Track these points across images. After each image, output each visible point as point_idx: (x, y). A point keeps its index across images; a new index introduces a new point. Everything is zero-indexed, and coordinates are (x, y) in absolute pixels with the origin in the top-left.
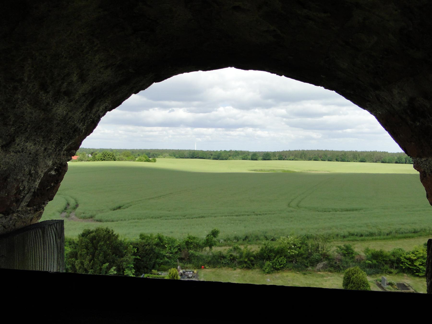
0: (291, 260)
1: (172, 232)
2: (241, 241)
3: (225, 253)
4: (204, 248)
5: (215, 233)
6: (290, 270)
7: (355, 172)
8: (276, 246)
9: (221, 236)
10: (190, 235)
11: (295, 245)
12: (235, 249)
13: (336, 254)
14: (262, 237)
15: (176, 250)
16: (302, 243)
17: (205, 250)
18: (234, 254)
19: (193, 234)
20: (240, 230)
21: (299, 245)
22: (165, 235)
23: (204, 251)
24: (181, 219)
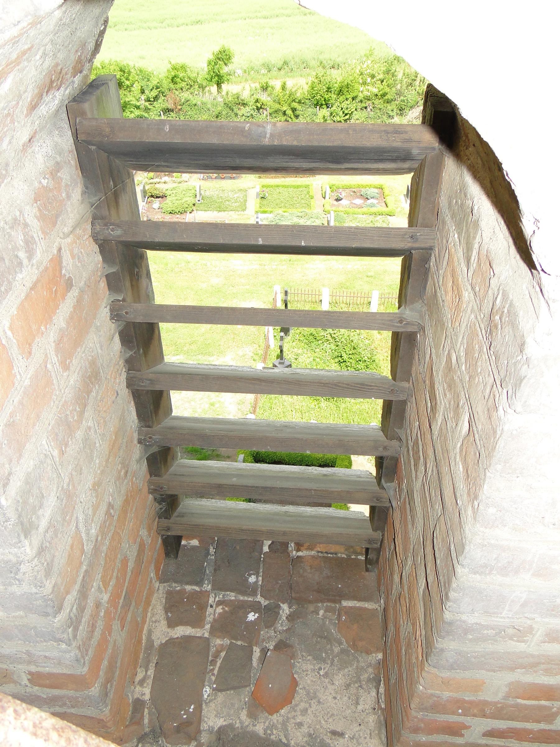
0: (364, 105)
1: (142, 58)
2: (274, 72)
3: (245, 96)
4: (207, 89)
5: (223, 57)
6: (203, 525)
7: (182, 304)
8: (337, 77)
9: (237, 65)
10: (173, 62)
11: (373, 76)
12: (265, 88)
13: (146, 126)
14: (313, 63)
15: (154, 93)
16: (388, 72)
17: (209, 91)
18: (264, 98)
19: (179, 61)
20: (274, 50)
21: (381, 76)
22: (131, 64)
23: (207, 94)
24: (156, 28)
